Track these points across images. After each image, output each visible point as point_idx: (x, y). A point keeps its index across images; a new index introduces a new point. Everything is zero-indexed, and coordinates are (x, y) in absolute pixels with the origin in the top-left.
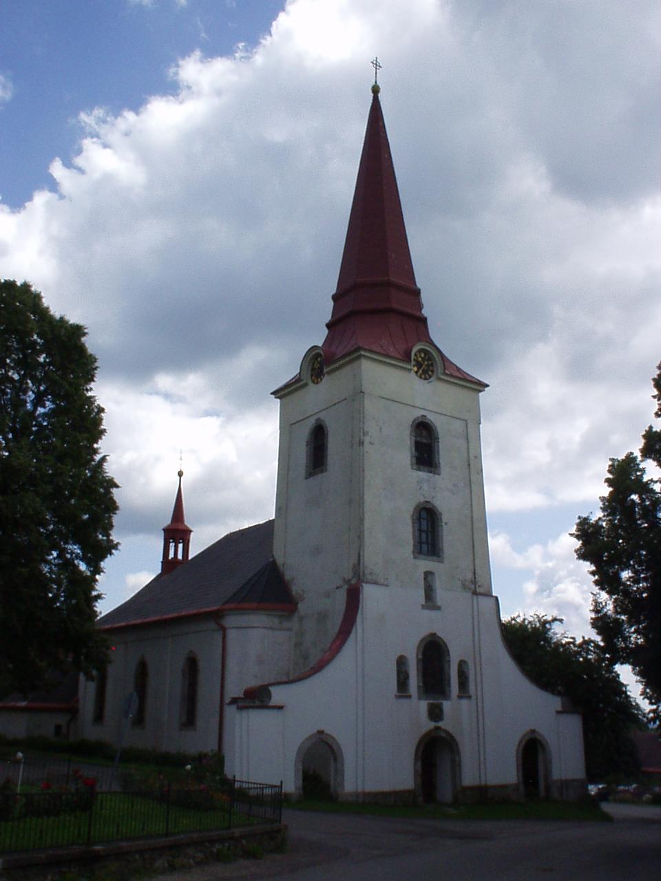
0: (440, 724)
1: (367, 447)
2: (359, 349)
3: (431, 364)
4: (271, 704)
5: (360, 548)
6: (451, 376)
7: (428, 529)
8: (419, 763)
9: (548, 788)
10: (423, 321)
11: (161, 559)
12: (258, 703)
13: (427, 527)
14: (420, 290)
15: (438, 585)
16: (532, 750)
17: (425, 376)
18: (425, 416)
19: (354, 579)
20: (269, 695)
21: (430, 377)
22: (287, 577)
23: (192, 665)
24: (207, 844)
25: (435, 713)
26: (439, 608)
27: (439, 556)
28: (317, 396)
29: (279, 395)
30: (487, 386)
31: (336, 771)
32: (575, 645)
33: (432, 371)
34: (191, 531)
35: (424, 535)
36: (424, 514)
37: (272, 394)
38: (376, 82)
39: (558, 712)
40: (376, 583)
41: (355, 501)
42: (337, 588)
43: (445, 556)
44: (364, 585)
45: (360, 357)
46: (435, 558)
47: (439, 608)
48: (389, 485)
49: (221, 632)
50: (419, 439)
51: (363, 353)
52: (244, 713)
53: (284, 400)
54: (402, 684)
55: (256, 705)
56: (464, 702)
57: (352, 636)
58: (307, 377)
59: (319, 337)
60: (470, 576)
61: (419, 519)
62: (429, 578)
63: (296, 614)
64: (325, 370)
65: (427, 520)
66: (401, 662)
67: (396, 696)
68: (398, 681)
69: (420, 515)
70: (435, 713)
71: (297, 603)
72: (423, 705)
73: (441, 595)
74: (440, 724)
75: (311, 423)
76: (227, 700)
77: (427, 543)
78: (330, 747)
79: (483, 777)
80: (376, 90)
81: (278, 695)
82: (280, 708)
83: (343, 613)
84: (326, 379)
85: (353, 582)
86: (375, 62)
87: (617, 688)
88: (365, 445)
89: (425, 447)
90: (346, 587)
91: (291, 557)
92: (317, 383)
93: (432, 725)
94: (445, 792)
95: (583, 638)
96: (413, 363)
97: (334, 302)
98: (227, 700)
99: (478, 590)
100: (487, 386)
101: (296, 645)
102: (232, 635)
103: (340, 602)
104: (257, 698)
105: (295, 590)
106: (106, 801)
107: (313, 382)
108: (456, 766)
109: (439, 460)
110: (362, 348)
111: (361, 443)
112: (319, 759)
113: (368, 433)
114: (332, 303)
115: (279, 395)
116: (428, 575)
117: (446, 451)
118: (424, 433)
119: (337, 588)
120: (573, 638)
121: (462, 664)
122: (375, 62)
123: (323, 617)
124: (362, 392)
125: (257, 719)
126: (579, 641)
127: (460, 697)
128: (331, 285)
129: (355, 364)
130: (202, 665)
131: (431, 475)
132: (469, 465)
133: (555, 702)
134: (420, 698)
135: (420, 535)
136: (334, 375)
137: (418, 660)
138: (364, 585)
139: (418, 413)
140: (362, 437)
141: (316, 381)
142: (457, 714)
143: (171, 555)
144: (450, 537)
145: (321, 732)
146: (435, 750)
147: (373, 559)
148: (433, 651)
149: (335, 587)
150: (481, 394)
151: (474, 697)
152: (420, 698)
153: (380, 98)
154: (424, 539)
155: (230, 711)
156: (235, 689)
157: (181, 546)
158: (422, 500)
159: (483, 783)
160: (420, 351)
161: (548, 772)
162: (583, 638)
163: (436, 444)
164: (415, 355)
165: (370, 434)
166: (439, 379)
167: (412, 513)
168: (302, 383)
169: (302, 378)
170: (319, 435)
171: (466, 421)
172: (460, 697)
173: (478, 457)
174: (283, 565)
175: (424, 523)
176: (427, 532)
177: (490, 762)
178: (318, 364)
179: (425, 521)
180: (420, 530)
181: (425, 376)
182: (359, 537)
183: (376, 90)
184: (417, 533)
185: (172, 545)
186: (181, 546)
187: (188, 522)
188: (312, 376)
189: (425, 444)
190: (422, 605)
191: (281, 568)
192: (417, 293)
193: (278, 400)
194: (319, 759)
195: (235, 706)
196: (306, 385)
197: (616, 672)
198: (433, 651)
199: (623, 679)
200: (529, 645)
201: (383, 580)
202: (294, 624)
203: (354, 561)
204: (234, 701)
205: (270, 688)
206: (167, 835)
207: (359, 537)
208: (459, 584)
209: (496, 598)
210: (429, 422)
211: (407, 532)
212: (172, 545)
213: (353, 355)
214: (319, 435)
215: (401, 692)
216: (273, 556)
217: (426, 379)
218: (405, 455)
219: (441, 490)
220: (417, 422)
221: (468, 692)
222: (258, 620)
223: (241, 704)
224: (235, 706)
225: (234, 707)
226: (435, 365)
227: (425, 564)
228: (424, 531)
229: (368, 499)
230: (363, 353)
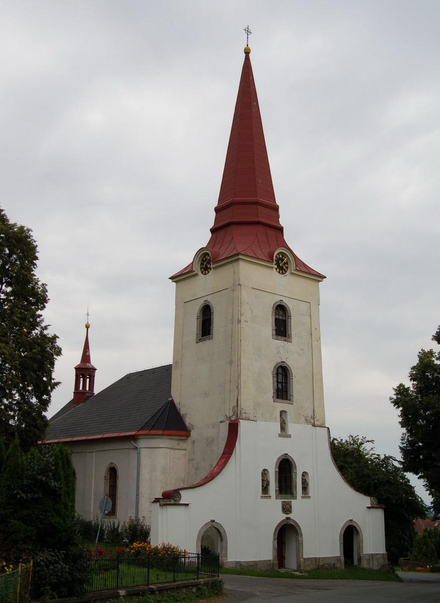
1: (243, 324)
2: (237, 254)
3: (284, 262)
4: (181, 502)
5: (238, 396)
6: (300, 271)
7: (282, 380)
8: (276, 541)
9: (360, 560)
10: (281, 230)
11: (73, 390)
12: (172, 502)
14: (278, 206)
15: (289, 418)
16: (350, 534)
17: (283, 272)
18: (282, 301)
19: (234, 417)
21: (286, 272)
22: (182, 412)
23: (113, 473)
24: (191, 587)
25: (287, 509)
26: (289, 436)
27: (290, 400)
28: (205, 286)
29: (175, 280)
30: (325, 277)
31: (222, 548)
32: (379, 459)
33: (287, 268)
34: (96, 370)
36: (280, 371)
37: (169, 278)
38: (247, 45)
39: (368, 508)
40: (248, 419)
41: (233, 361)
42: (221, 422)
43: (294, 399)
44: (240, 420)
45: (238, 260)
46: (285, 401)
47: (289, 436)
48: (259, 351)
50: (277, 317)
51: (241, 257)
52: (164, 508)
53: (180, 284)
54: (265, 489)
55: (171, 503)
58: (197, 269)
59: (203, 238)
60: (310, 414)
61: (277, 374)
62: (283, 416)
63: (190, 438)
64: (212, 266)
65: (282, 374)
66: (265, 473)
67: (261, 496)
69: (277, 371)
70: (287, 509)
72: (279, 502)
73: (291, 428)
75: (199, 304)
78: (219, 531)
80: (247, 52)
81: (185, 496)
82: (187, 505)
84: (212, 272)
85: (233, 418)
86: (249, 33)
87: (410, 490)
88: (241, 323)
90: (228, 422)
91: (181, 394)
92: (205, 274)
93: (284, 516)
94: (291, 563)
95: (385, 455)
96: (275, 262)
97: (216, 213)
99: (316, 423)
100: (325, 277)
101: (190, 460)
102: (144, 453)
104: (170, 498)
105: (187, 421)
107: (202, 273)
108: (299, 545)
109: (291, 332)
110: (241, 254)
111: (239, 321)
112: (212, 537)
113: (243, 314)
114: (214, 214)
115: (175, 280)
116: (282, 413)
117: (296, 325)
118: (281, 313)
119: (221, 422)
120: (378, 455)
121: (305, 474)
122: (247, 29)
123: (210, 442)
124: (239, 285)
125: (172, 512)
126: (382, 457)
128: (214, 200)
129: (235, 264)
130: (120, 473)
131: (286, 343)
132: (312, 335)
133: (366, 501)
134: (276, 498)
135: (278, 384)
136: (218, 270)
138: (240, 420)
139: (276, 299)
140: (240, 317)
141: (204, 272)
142: (302, 511)
144: (297, 386)
145: (213, 521)
146: (286, 533)
147: (246, 404)
148: (286, 466)
149: (219, 421)
150: (320, 283)
152: (276, 498)
153: (251, 58)
158: (279, 361)
160: (278, 254)
161: (360, 548)
162: (385, 455)
163: (289, 320)
164: (276, 257)
165: (245, 314)
166: (292, 274)
167: (272, 371)
168: (194, 273)
169: (194, 269)
170: (206, 312)
171: (310, 303)
173: (318, 329)
175: (280, 376)
177: (320, 543)
178: (206, 260)
179: (281, 375)
180: (277, 382)
181: (283, 272)
182: (237, 388)
183: (247, 52)
184: (276, 383)
187: (94, 362)
188: (201, 268)
189: (281, 320)
190: (279, 434)
192: (276, 209)
193: (175, 283)
194: (212, 537)
195: (159, 504)
196: (196, 275)
197: (407, 479)
198: (286, 466)
199: (412, 483)
200: (350, 460)
201: (253, 418)
202: (187, 445)
205: (180, 492)
206: (174, 582)
207: (237, 388)
208: (303, 419)
209: (328, 428)
210: (285, 305)
213: (234, 258)
214: (206, 312)
215: (265, 494)
216: (171, 397)
217: (283, 274)
218: (269, 328)
219: (288, 352)
220: (276, 305)
222: (163, 443)
223: (162, 503)
224: (159, 504)
226: (289, 263)
227: (281, 405)
228: (280, 382)
229: (243, 361)
230: (241, 257)
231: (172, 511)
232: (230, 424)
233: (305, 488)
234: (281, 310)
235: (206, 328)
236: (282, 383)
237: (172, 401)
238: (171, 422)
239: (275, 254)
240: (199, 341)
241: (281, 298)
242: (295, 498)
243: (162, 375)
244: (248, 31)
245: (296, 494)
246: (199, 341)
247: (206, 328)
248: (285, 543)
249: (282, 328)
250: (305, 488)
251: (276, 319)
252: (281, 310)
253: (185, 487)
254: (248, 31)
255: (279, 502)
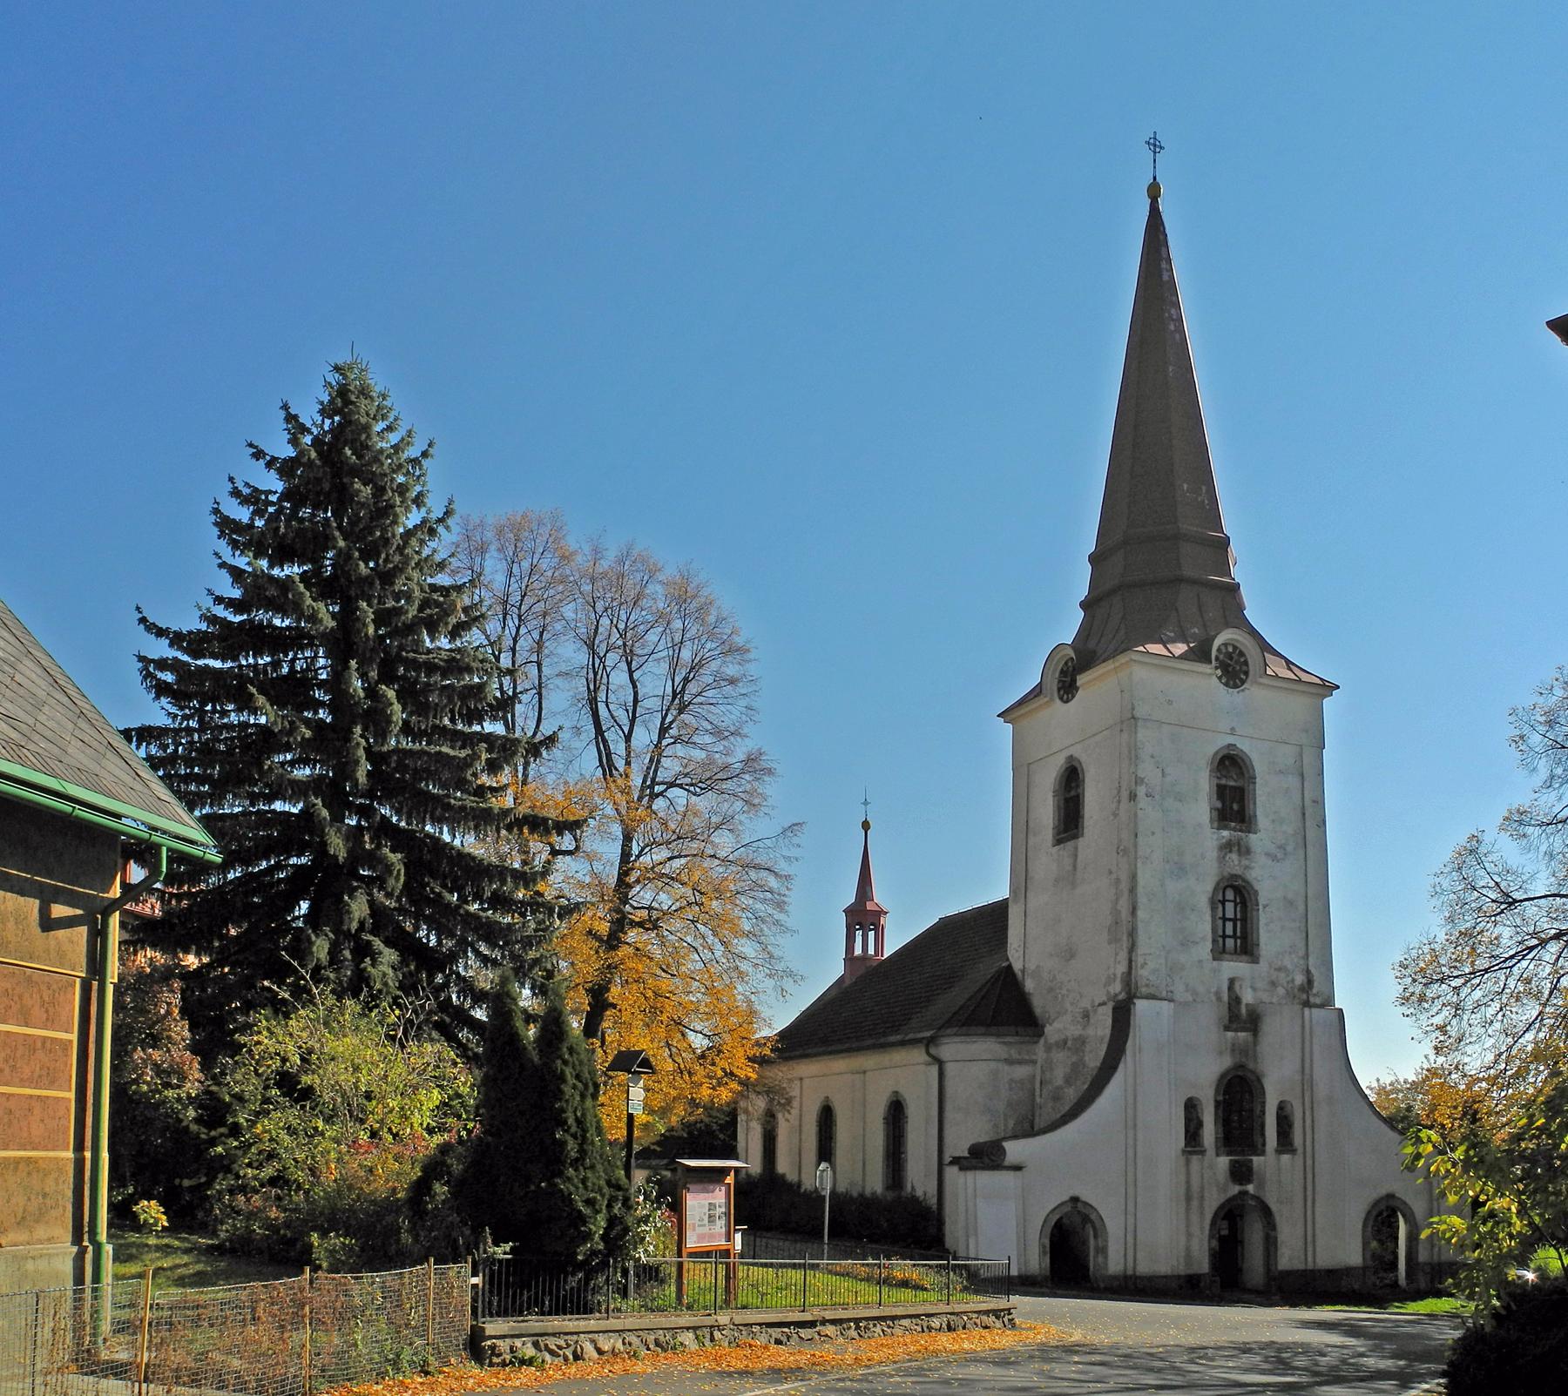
0: (1250, 1188)
4: (1006, 1163)
13: (1237, 915)
20: (1003, 1152)
21: (1243, 682)
28: (1064, 727)
33: (1246, 673)
35: (1229, 925)
36: (1230, 895)
46: (1244, 957)
49: (934, 1070)
50: (1223, 782)
56: (1285, 1158)
57: (1121, 1066)
63: (1042, 1041)
66: (1191, 1107)
68: (1187, 1131)
70: (1241, 1173)
71: (1043, 1027)
72: (1224, 1162)
74: (1250, 1188)
76: (947, 1159)
77: (1234, 936)
79: (1310, 1259)
80: (1154, 192)
81: (1015, 1150)
83: (1107, 1039)
89: (1233, 801)
90: (1111, 1005)
91: (1026, 951)
93: (1236, 1189)
98: (947, 1159)
103: (1102, 1025)
104: (985, 1156)
105: (1038, 1004)
106: (327, 1163)
107: (1061, 698)
117: (1270, 800)
121: (1281, 1107)
127: (1279, 1152)
137: (1217, 1104)
143: (858, 951)
145: (1075, 1200)
148: (1239, 1093)
151: (1300, 1151)
154: (1229, 931)
155: (952, 1172)
156: (958, 1145)
157: (871, 934)
159: (1310, 1266)
160: (1225, 645)
170: (1072, 777)
172: (1279, 1152)
174: (1023, 971)
175: (1230, 907)
176: (1234, 920)
178: (1067, 675)
183: (1154, 192)
185: (859, 934)
186: (871, 934)
187: (880, 896)
191: (1019, 974)
198: (1239, 1093)
203: (1121, 969)
204: (956, 1161)
211: (1203, 926)
212: (859, 934)
214: (1072, 777)
217: (1235, 686)
218: (1201, 808)
221: (1291, 1144)
225: (955, 1169)
231: (984, 1179)
232: (1115, 1009)
233: (1285, 1141)
234: (1230, 764)
235: (1070, 821)
236: (1234, 920)
237: (1010, 967)
238: (1007, 1009)
239: (1217, 643)
240: (1058, 841)
241: (1230, 740)
242: (1263, 1153)
243: (990, 922)
244: (1155, 146)
245: (1264, 1145)
246: (1058, 841)
247: (1070, 821)
248: (1242, 1242)
249: (1233, 801)
250: (1285, 1141)
251: (1219, 786)
252: (1230, 764)
253: (1144, 1268)
254: (1155, 146)
255: (1224, 1162)
